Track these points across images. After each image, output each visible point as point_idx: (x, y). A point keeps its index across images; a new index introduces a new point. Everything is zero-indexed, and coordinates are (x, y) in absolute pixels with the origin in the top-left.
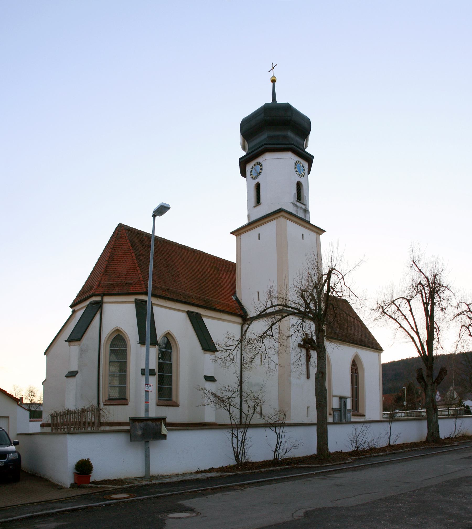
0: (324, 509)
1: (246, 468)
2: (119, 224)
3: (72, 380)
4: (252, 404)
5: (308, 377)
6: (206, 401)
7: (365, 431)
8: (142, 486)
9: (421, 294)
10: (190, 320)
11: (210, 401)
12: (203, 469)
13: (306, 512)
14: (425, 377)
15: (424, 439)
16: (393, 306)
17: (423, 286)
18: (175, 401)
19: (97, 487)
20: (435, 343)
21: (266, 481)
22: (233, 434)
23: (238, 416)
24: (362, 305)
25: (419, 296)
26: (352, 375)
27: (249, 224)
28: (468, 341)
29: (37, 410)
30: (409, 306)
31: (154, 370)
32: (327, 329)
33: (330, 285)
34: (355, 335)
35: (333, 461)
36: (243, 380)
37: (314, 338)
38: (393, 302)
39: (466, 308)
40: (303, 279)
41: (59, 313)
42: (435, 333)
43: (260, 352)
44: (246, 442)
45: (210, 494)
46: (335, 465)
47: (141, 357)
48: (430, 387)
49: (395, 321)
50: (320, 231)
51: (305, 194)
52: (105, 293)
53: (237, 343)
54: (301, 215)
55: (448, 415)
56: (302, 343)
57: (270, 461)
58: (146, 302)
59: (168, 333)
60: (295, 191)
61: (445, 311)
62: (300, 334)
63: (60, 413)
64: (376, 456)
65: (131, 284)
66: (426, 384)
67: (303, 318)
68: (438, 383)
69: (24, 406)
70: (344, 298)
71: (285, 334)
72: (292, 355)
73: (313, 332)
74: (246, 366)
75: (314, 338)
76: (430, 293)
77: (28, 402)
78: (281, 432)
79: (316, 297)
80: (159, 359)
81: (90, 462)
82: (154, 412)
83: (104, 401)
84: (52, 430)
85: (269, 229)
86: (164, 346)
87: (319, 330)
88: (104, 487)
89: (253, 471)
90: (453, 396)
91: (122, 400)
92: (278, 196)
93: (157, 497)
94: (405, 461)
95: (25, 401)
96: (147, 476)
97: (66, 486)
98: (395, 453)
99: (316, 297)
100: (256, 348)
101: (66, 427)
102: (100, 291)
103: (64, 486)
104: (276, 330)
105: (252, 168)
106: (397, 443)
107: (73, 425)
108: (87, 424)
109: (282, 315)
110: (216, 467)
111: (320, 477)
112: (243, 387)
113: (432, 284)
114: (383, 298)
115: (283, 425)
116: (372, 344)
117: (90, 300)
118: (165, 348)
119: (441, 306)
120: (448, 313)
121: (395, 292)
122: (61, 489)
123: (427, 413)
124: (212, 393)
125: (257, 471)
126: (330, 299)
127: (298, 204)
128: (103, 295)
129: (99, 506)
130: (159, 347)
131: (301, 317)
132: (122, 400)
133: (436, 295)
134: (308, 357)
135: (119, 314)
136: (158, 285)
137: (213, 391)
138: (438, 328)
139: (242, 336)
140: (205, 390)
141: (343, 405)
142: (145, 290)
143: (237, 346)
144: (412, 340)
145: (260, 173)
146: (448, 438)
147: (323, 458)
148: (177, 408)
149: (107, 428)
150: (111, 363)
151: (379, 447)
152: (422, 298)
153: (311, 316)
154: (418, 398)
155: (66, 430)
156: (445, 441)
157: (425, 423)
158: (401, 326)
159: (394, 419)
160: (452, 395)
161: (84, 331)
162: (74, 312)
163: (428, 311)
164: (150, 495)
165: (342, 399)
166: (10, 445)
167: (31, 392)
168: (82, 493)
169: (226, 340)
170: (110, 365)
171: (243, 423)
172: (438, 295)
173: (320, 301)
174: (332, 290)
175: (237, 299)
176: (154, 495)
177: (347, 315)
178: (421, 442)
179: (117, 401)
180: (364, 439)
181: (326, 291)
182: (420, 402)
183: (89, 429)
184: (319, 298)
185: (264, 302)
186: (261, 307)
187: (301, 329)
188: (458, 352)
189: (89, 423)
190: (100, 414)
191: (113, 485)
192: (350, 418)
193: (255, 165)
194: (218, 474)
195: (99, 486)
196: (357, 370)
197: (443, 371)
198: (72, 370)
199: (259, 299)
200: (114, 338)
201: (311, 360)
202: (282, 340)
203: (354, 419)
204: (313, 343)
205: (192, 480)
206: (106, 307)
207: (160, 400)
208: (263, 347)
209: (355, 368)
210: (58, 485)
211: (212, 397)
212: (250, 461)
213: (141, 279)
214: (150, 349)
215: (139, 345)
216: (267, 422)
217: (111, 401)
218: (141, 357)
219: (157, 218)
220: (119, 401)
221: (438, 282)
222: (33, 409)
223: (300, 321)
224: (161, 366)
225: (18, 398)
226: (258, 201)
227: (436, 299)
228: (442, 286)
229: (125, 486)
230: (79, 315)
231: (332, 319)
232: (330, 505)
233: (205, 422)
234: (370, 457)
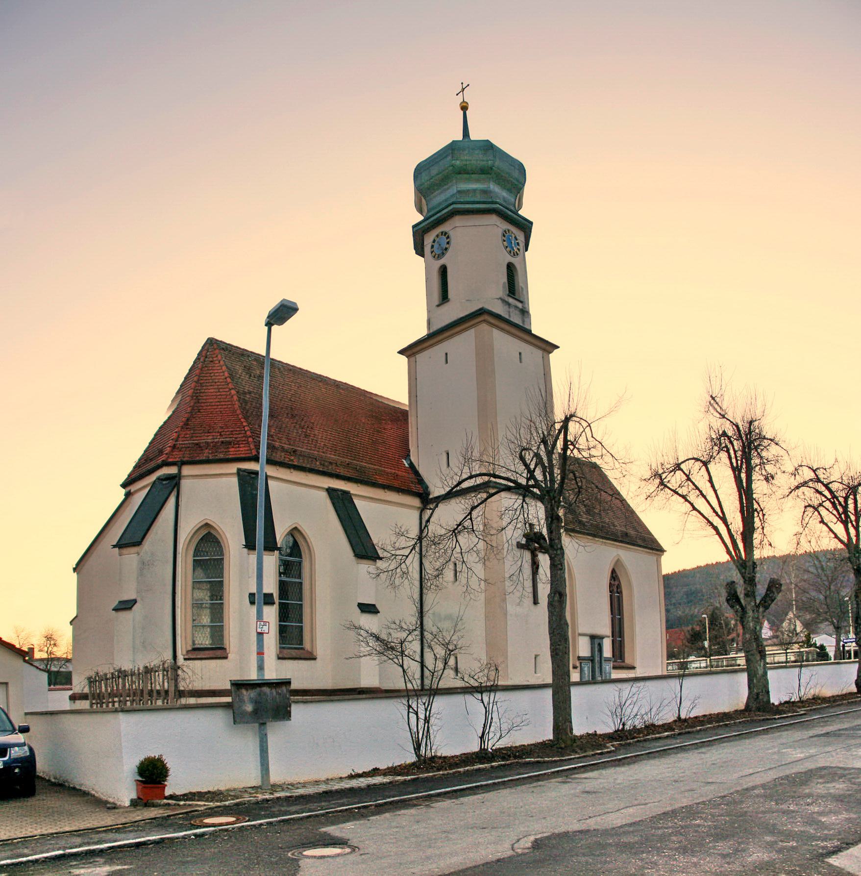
0: (566, 834)
1: (432, 767)
2: (208, 339)
3: (123, 615)
4: (440, 652)
5: (536, 602)
6: (362, 649)
7: (636, 696)
8: (257, 803)
9: (728, 451)
10: (333, 504)
11: (369, 648)
12: (360, 772)
13: (536, 840)
14: (741, 596)
15: (742, 706)
16: (679, 473)
17: (729, 438)
18: (310, 650)
19: (179, 805)
20: (757, 536)
21: (467, 788)
22: (409, 706)
23: (418, 675)
24: (625, 473)
25: (723, 455)
26: (611, 596)
27: (430, 336)
28: (818, 533)
29: (62, 670)
30: (706, 473)
31: (272, 595)
32: (565, 515)
33: (569, 438)
34: (614, 526)
35: (581, 749)
36: (425, 609)
37: (545, 532)
38: (678, 467)
39: (812, 475)
40: (522, 429)
41: (101, 497)
42: (756, 520)
43: (453, 559)
44: (432, 720)
45: (373, 814)
46: (584, 757)
47: (248, 573)
48: (750, 613)
49: (683, 500)
50: (548, 347)
51: (521, 284)
52: (185, 459)
53: (413, 542)
54: (516, 319)
55: (786, 662)
56: (524, 541)
57: (474, 753)
58: (256, 473)
59: (296, 528)
60: (504, 279)
61: (773, 482)
62: (519, 525)
63: (106, 675)
64: (656, 739)
65: (230, 443)
66: (743, 609)
67: (524, 497)
68: (766, 608)
69: (36, 664)
70: (593, 460)
71: (495, 525)
72: (508, 563)
73: (542, 522)
74: (429, 584)
75: (545, 532)
76: (743, 451)
77: (44, 656)
78: (491, 701)
79: (545, 459)
80: (280, 576)
81: (163, 762)
82: (274, 670)
83: (184, 653)
84: (92, 705)
85: (462, 345)
86: (288, 551)
87: (552, 518)
88: (190, 805)
89: (446, 772)
90: (795, 629)
91: (217, 651)
92: (479, 289)
93: (283, 821)
94: (708, 746)
95: (38, 655)
96: (266, 785)
97: (123, 804)
98: (689, 732)
99: (545, 459)
100: (446, 551)
101: (116, 699)
102: (177, 456)
103: (119, 803)
104: (479, 519)
105: (434, 241)
106: (692, 715)
107: (129, 696)
108: (155, 694)
109: (488, 492)
110: (383, 766)
111: (560, 779)
112: (425, 622)
113: (746, 435)
114: (660, 460)
115: (494, 689)
116: (644, 540)
117: (159, 472)
118: (290, 555)
119: (764, 472)
120: (779, 485)
121: (680, 448)
122: (114, 808)
123: (747, 661)
124: (372, 635)
125: (451, 772)
126: (568, 463)
127: (511, 300)
128: (181, 464)
129: (184, 837)
130: (280, 553)
131: (520, 494)
132: (217, 651)
133: (754, 453)
134: (535, 566)
135: (210, 497)
136: (277, 444)
137: (374, 631)
138: (762, 510)
139: (421, 531)
140: (361, 628)
141: (596, 650)
142: (254, 453)
143: (414, 548)
144: (715, 533)
145: (446, 249)
146: (786, 702)
147: (563, 746)
148: (313, 662)
149: (192, 701)
150: (196, 584)
151: (660, 723)
152: (730, 458)
153: (538, 492)
154: (729, 633)
155: (117, 705)
156: (780, 708)
157: (743, 678)
158: (694, 509)
159: (687, 672)
160: (793, 627)
161: (146, 528)
162: (128, 495)
163: (741, 481)
164: (272, 817)
165: (595, 640)
166: (13, 731)
167: (49, 638)
168: (152, 815)
169: (394, 539)
170: (193, 588)
171: (427, 687)
172: (758, 454)
173: (551, 466)
174: (571, 447)
175: (412, 465)
176: (279, 819)
177: (600, 490)
178: (736, 711)
179: (207, 652)
180: (635, 710)
181: (562, 449)
182: (733, 640)
183: (159, 703)
184: (550, 460)
185: (456, 470)
186: (452, 478)
187: (522, 516)
188: (801, 551)
189: (158, 692)
190: (178, 675)
191: (207, 801)
192: (610, 674)
193: (437, 236)
194: (386, 780)
195: (182, 803)
196: (619, 586)
197: (774, 586)
198: (125, 598)
199: (448, 465)
200: (202, 539)
201: (541, 570)
202: (489, 537)
203: (615, 675)
204: (542, 541)
205: (342, 790)
206: (185, 484)
207: (284, 648)
208: (458, 549)
209: (616, 583)
210: (107, 802)
211: (372, 642)
212: (439, 754)
213: (248, 433)
214: (264, 557)
215: (246, 550)
216: (467, 685)
217: (197, 653)
218: (248, 573)
219: (275, 328)
220: (211, 652)
221: (757, 431)
222: (54, 669)
223: (520, 501)
224: (283, 587)
225: (25, 649)
226: (444, 297)
227: (756, 461)
228: (764, 438)
229: (227, 803)
230: (138, 499)
231: (574, 498)
232: (577, 827)
233: (362, 686)
234: (645, 740)
